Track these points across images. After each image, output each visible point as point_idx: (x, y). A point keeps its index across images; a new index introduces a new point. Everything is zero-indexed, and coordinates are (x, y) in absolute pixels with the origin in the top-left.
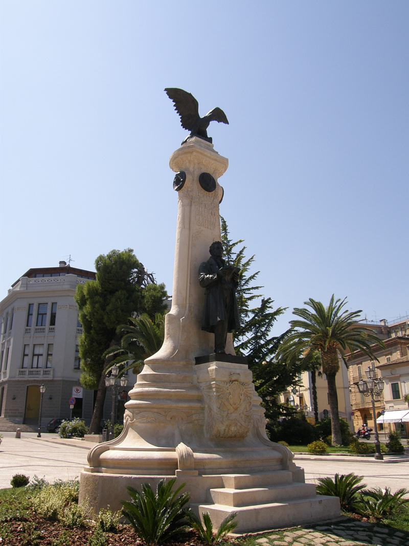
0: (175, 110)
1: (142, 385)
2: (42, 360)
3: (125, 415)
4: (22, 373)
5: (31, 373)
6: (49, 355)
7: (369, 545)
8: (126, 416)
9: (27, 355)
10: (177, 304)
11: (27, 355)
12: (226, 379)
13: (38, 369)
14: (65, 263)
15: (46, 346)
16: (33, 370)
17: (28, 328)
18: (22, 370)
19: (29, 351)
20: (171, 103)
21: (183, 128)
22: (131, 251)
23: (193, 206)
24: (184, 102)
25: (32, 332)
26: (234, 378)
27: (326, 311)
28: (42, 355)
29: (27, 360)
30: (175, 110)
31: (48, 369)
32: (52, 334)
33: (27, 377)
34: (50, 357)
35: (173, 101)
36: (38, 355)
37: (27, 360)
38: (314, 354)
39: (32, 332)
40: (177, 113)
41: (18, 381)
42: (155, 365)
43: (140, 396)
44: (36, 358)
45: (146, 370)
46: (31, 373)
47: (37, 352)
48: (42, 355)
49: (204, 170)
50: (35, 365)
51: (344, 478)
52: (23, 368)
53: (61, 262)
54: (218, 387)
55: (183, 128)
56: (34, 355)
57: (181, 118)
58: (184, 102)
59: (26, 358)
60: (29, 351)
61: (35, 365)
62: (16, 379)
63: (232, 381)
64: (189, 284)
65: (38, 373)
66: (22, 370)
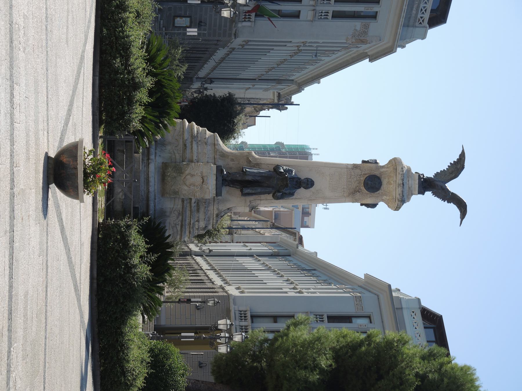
0: (451, 163)
12: (204, 174)
17: (326, 319)
18: (249, 315)
20: (455, 157)
24: (457, 168)
30: (451, 163)
43: (191, 129)
49: (385, 182)
52: (252, 317)
66: (249, 315)
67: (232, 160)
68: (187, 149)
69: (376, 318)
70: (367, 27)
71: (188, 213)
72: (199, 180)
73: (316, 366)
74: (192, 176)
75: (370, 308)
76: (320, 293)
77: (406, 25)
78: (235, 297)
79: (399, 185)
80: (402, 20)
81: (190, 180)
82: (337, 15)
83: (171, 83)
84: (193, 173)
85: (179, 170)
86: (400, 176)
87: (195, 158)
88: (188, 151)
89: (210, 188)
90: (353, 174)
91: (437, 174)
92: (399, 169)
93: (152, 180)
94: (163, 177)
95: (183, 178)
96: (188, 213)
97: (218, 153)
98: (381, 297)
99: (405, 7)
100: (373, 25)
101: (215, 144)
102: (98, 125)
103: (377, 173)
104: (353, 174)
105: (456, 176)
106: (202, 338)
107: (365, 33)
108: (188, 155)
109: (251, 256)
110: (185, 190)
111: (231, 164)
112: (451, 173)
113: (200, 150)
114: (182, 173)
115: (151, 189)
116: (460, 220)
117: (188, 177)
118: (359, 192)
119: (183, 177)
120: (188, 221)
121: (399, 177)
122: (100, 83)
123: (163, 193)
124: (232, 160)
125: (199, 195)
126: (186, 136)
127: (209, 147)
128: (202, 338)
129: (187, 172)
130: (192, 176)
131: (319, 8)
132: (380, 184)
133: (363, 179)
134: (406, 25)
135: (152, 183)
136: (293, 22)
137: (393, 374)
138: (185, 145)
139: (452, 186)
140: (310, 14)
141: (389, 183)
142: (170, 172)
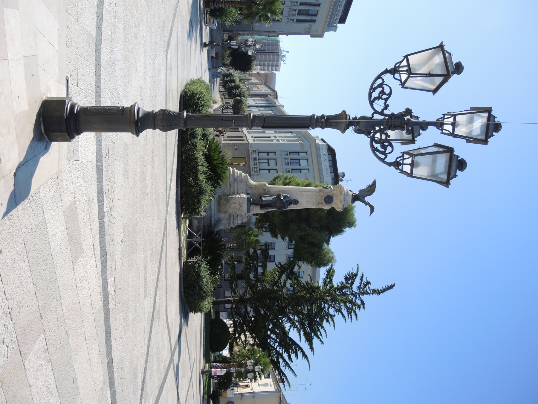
1: (237, 173)
2: (265, 166)
4: (254, 152)
5: (255, 159)
6: (269, 170)
9: (268, 155)
10: (270, 188)
11: (268, 155)
13: (258, 164)
14: (343, 176)
15: (276, 167)
16: (257, 160)
18: (257, 152)
19: (271, 156)
20: (371, 183)
22: (355, 227)
24: (371, 189)
25: (286, 157)
28: (269, 165)
29: (264, 155)
31: (258, 170)
32: (285, 171)
33: (252, 156)
34: (268, 171)
36: (268, 163)
37: (264, 155)
38: (215, 21)
39: (286, 157)
41: (248, 150)
42: (246, 176)
43: (234, 172)
44: (266, 161)
45: (243, 174)
46: (255, 159)
47: (271, 161)
48: (269, 165)
49: (335, 199)
50: (261, 161)
51: (233, 84)
52: (258, 152)
53: (343, 174)
56: (268, 160)
58: (371, 189)
59: (266, 154)
60: (271, 156)
61: (261, 161)
62: (250, 149)
65: (255, 164)
66: (257, 152)
67: (256, 189)
69: (309, 153)
70: (311, 26)
71: (232, 218)
72: (238, 206)
74: (235, 203)
75: (307, 149)
76: (288, 141)
77: (328, 26)
78: (251, 144)
80: (327, 24)
81: (233, 206)
82: (298, 21)
83: (222, 166)
85: (228, 201)
87: (236, 191)
91: (361, 191)
92: (343, 193)
93: (213, 208)
94: (219, 203)
96: (232, 218)
98: (312, 144)
99: (328, 19)
100: (314, 25)
101: (246, 181)
102: (180, 211)
103: (331, 194)
105: (370, 194)
107: (310, 29)
108: (232, 190)
109: (257, 106)
110: (231, 210)
111: (255, 191)
112: (368, 191)
115: (213, 212)
116: (370, 212)
120: (232, 221)
121: (342, 197)
122: (181, 192)
123: (219, 211)
124: (256, 189)
125: (237, 213)
126: (231, 179)
127: (243, 184)
130: (235, 203)
131: (290, 18)
132: (332, 200)
133: (324, 197)
134: (328, 26)
135: (213, 210)
136: (278, 23)
139: (367, 199)
140: (286, 20)
142: (222, 201)
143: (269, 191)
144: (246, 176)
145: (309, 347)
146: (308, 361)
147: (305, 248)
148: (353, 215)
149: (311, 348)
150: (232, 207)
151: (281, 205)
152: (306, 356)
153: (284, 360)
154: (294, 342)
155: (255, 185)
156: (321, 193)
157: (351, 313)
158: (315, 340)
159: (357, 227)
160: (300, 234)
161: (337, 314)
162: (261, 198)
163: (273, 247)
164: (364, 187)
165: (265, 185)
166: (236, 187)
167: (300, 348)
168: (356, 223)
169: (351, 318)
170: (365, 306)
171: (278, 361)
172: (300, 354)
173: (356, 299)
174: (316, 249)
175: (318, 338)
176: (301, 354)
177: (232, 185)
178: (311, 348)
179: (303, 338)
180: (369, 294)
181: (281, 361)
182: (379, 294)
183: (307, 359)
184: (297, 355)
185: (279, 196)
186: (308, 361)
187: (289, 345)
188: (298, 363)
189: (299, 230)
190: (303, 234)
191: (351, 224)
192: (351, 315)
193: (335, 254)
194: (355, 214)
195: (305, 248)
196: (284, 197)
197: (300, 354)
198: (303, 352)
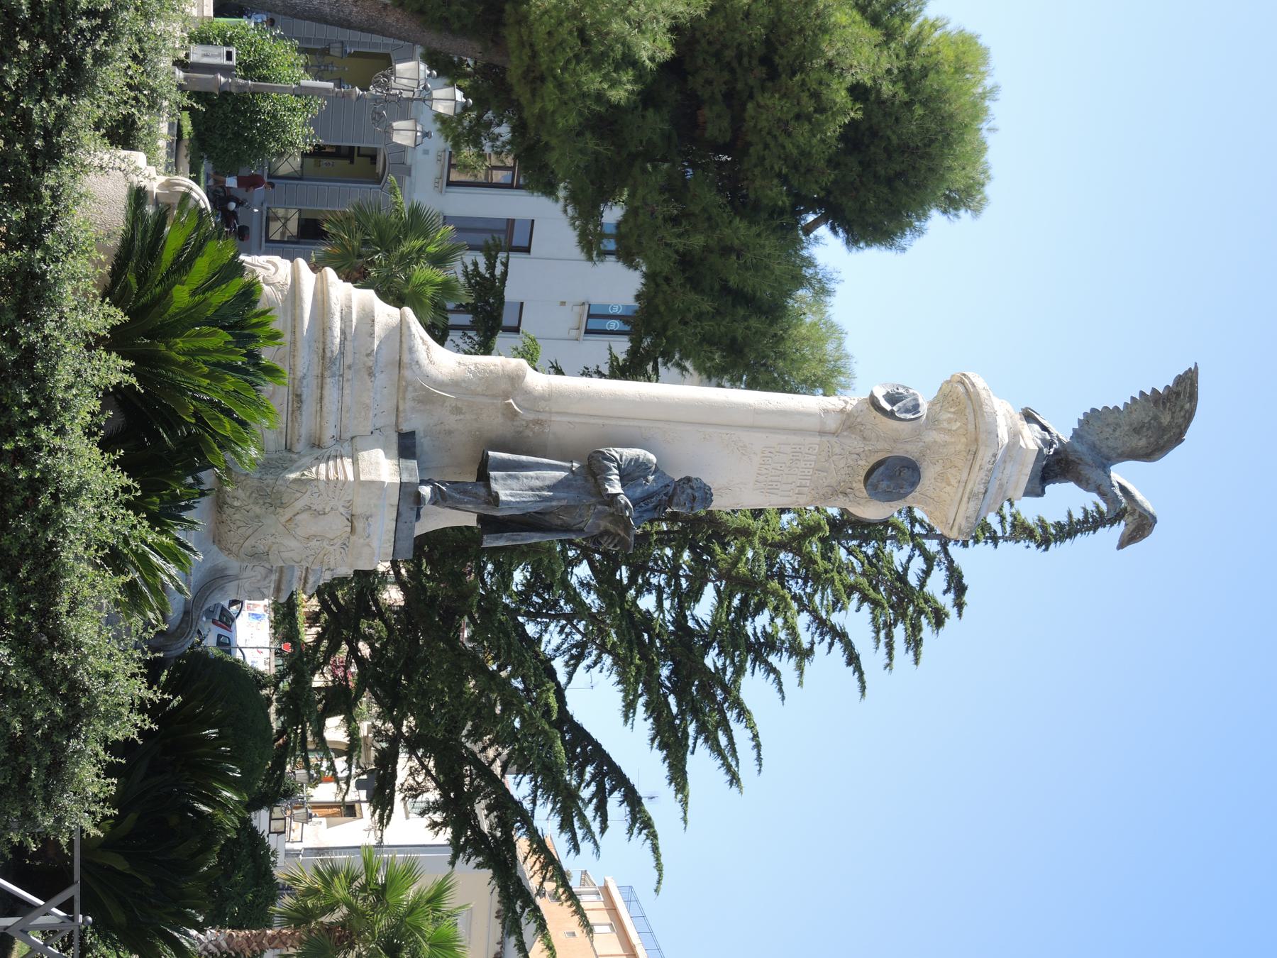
3: (276, 259)
7: (980, 383)
8: (274, 265)
10: (549, 397)
12: (358, 510)
20: (1163, 380)
21: (1085, 414)
22: (977, 211)
23: (817, 439)
24: (1162, 419)
26: (359, 525)
27: (172, 310)
30: (1142, 393)
35: (1079, 420)
40: (1133, 398)
42: (401, 329)
49: (929, 474)
54: (339, 485)
55: (1085, 414)
57: (1116, 408)
58: (1162, 419)
63: (351, 519)
64: (600, 421)
68: (304, 407)
73: (629, 60)
79: (972, 496)
81: (307, 525)
84: (319, 508)
86: (982, 474)
87: (329, 432)
88: (309, 406)
89: (375, 544)
90: (837, 450)
91: (1093, 418)
95: (283, 520)
97: (410, 395)
101: (402, 360)
104: (837, 450)
106: (354, 97)
111: (452, 421)
112: (1137, 430)
113: (348, 399)
114: (282, 505)
117: (304, 517)
118: (845, 494)
119: (287, 517)
124: (457, 410)
127: (381, 379)
128: (354, 97)
129: (299, 504)
133: (865, 465)
137: (803, 83)
138: (298, 397)
141: (941, 476)
143: (538, 422)
144: (403, 322)
145: (664, 770)
146: (655, 849)
147: (700, 316)
148: (981, 149)
149: (678, 776)
150: (300, 532)
151: (604, 524)
152: (647, 824)
153: (539, 845)
154: (597, 746)
155: (455, 385)
156: (854, 443)
157: (889, 627)
158: (700, 761)
159: (987, 212)
160: (679, 244)
161: (820, 649)
162: (483, 477)
163: (518, 240)
164: (1117, 393)
165: (515, 379)
166: (333, 408)
167: (621, 781)
168: (989, 190)
169: (890, 646)
170: (967, 598)
171: (511, 846)
172: (616, 808)
173: (927, 573)
174: (754, 323)
175: (716, 748)
176: (625, 809)
177: (309, 394)
178: (678, 776)
179: (643, 724)
180: (995, 539)
181: (522, 844)
182: (1045, 542)
183: (653, 836)
184: (601, 809)
185: (594, 467)
186: (655, 849)
187: (571, 769)
188: (607, 860)
189: (675, 220)
190: (697, 241)
191: (961, 198)
192: (889, 636)
193: (850, 345)
194: (991, 140)
195: (700, 316)
196: (631, 473)
197: (616, 808)
198: (633, 799)
